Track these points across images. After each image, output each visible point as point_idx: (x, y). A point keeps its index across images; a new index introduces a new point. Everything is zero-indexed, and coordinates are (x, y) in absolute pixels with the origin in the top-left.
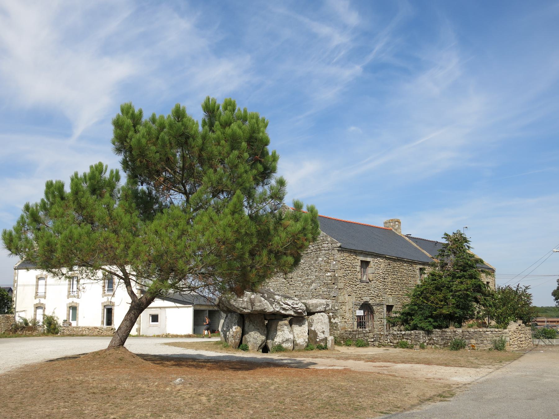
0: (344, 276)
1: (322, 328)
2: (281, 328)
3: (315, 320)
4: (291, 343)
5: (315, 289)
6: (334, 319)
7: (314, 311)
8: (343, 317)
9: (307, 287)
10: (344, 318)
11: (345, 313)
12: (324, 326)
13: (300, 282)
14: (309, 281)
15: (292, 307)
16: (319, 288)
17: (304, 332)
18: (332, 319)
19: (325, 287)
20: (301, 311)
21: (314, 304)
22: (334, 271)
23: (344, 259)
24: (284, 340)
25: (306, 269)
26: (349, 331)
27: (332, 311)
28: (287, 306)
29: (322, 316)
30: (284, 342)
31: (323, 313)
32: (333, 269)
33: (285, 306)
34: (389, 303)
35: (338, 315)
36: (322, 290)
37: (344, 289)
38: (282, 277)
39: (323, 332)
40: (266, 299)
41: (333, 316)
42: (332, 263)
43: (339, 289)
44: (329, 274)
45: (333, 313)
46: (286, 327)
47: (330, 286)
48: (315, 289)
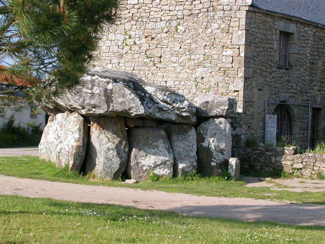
17: (191, 150)
24: (157, 163)
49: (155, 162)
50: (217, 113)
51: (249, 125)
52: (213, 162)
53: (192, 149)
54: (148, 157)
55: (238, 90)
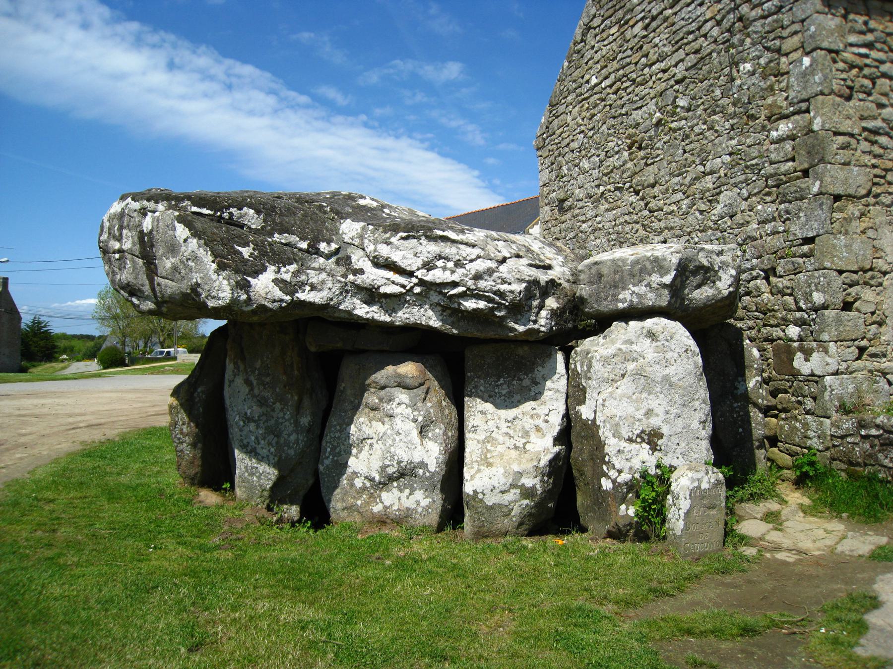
0: (876, 132)
1: (639, 415)
2: (381, 400)
3: (597, 366)
4: (427, 490)
5: (731, 217)
6: (807, 354)
7: (605, 306)
8: (862, 350)
9: (701, 212)
10: (872, 350)
11: (880, 324)
12: (658, 403)
13: (679, 196)
14: (708, 182)
15: (421, 282)
16: (744, 205)
17: (538, 428)
18: (799, 355)
19: (768, 199)
20: (482, 304)
21: (605, 271)
22: (804, 106)
23: (870, 45)
24: (390, 471)
25: (697, 130)
26: (878, 427)
27: (798, 315)
28: (390, 275)
29: (651, 335)
30: (391, 479)
31: (663, 321)
32: (800, 97)
33: (373, 276)
34: (579, 434)
35: (825, 337)
36: (757, 213)
37: (871, 200)
38: (628, 185)
39: (652, 438)
40: (194, 235)
41: (801, 339)
42: (795, 71)
43: (837, 198)
44: (784, 128)
45: (801, 323)
46: (403, 396)
47: (789, 188)
48: (731, 217)
49: (384, 468)
50: (635, 300)
51: (864, 343)
52: (608, 477)
53: (543, 425)
54: (367, 448)
55: (810, 235)
